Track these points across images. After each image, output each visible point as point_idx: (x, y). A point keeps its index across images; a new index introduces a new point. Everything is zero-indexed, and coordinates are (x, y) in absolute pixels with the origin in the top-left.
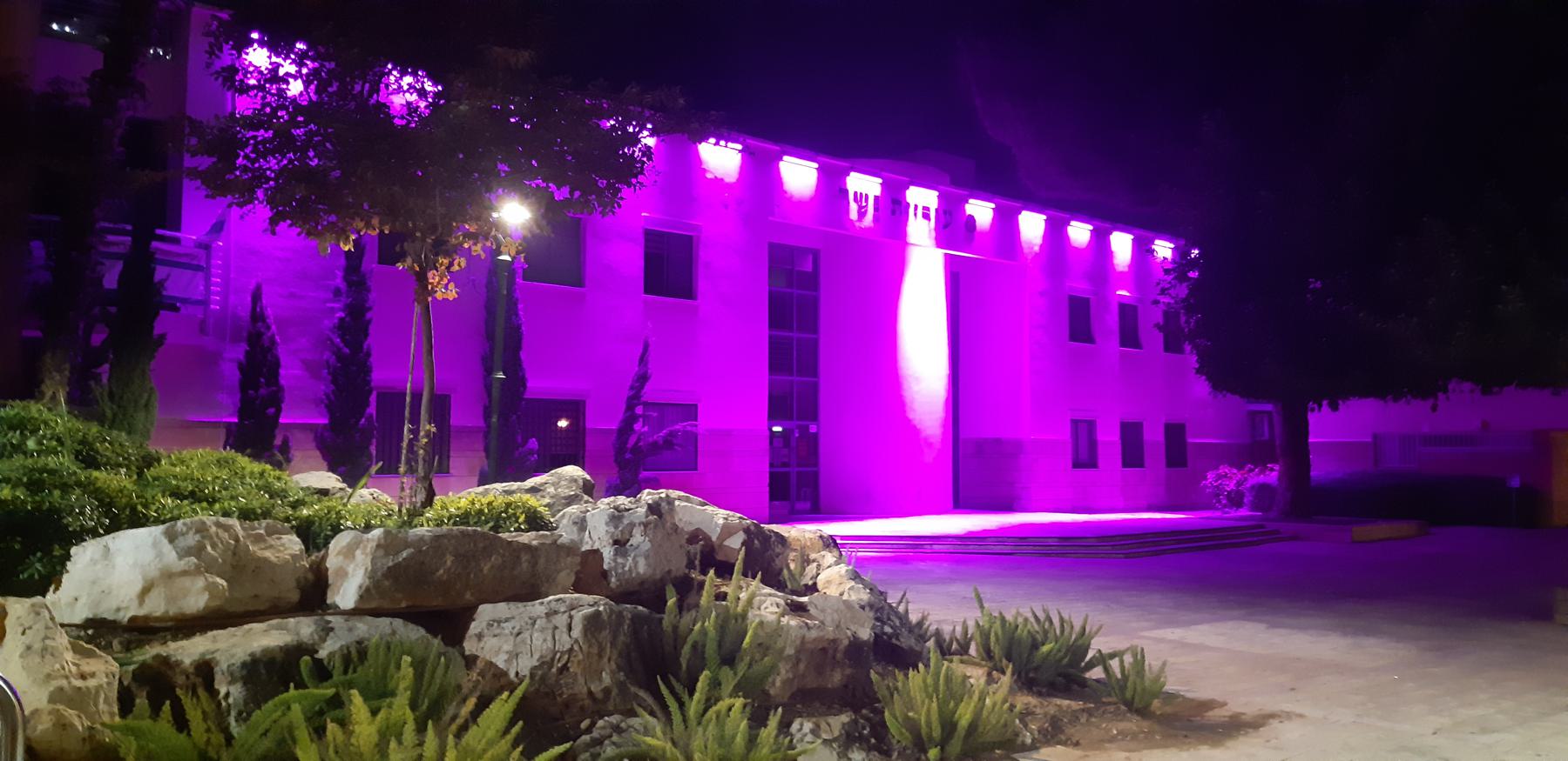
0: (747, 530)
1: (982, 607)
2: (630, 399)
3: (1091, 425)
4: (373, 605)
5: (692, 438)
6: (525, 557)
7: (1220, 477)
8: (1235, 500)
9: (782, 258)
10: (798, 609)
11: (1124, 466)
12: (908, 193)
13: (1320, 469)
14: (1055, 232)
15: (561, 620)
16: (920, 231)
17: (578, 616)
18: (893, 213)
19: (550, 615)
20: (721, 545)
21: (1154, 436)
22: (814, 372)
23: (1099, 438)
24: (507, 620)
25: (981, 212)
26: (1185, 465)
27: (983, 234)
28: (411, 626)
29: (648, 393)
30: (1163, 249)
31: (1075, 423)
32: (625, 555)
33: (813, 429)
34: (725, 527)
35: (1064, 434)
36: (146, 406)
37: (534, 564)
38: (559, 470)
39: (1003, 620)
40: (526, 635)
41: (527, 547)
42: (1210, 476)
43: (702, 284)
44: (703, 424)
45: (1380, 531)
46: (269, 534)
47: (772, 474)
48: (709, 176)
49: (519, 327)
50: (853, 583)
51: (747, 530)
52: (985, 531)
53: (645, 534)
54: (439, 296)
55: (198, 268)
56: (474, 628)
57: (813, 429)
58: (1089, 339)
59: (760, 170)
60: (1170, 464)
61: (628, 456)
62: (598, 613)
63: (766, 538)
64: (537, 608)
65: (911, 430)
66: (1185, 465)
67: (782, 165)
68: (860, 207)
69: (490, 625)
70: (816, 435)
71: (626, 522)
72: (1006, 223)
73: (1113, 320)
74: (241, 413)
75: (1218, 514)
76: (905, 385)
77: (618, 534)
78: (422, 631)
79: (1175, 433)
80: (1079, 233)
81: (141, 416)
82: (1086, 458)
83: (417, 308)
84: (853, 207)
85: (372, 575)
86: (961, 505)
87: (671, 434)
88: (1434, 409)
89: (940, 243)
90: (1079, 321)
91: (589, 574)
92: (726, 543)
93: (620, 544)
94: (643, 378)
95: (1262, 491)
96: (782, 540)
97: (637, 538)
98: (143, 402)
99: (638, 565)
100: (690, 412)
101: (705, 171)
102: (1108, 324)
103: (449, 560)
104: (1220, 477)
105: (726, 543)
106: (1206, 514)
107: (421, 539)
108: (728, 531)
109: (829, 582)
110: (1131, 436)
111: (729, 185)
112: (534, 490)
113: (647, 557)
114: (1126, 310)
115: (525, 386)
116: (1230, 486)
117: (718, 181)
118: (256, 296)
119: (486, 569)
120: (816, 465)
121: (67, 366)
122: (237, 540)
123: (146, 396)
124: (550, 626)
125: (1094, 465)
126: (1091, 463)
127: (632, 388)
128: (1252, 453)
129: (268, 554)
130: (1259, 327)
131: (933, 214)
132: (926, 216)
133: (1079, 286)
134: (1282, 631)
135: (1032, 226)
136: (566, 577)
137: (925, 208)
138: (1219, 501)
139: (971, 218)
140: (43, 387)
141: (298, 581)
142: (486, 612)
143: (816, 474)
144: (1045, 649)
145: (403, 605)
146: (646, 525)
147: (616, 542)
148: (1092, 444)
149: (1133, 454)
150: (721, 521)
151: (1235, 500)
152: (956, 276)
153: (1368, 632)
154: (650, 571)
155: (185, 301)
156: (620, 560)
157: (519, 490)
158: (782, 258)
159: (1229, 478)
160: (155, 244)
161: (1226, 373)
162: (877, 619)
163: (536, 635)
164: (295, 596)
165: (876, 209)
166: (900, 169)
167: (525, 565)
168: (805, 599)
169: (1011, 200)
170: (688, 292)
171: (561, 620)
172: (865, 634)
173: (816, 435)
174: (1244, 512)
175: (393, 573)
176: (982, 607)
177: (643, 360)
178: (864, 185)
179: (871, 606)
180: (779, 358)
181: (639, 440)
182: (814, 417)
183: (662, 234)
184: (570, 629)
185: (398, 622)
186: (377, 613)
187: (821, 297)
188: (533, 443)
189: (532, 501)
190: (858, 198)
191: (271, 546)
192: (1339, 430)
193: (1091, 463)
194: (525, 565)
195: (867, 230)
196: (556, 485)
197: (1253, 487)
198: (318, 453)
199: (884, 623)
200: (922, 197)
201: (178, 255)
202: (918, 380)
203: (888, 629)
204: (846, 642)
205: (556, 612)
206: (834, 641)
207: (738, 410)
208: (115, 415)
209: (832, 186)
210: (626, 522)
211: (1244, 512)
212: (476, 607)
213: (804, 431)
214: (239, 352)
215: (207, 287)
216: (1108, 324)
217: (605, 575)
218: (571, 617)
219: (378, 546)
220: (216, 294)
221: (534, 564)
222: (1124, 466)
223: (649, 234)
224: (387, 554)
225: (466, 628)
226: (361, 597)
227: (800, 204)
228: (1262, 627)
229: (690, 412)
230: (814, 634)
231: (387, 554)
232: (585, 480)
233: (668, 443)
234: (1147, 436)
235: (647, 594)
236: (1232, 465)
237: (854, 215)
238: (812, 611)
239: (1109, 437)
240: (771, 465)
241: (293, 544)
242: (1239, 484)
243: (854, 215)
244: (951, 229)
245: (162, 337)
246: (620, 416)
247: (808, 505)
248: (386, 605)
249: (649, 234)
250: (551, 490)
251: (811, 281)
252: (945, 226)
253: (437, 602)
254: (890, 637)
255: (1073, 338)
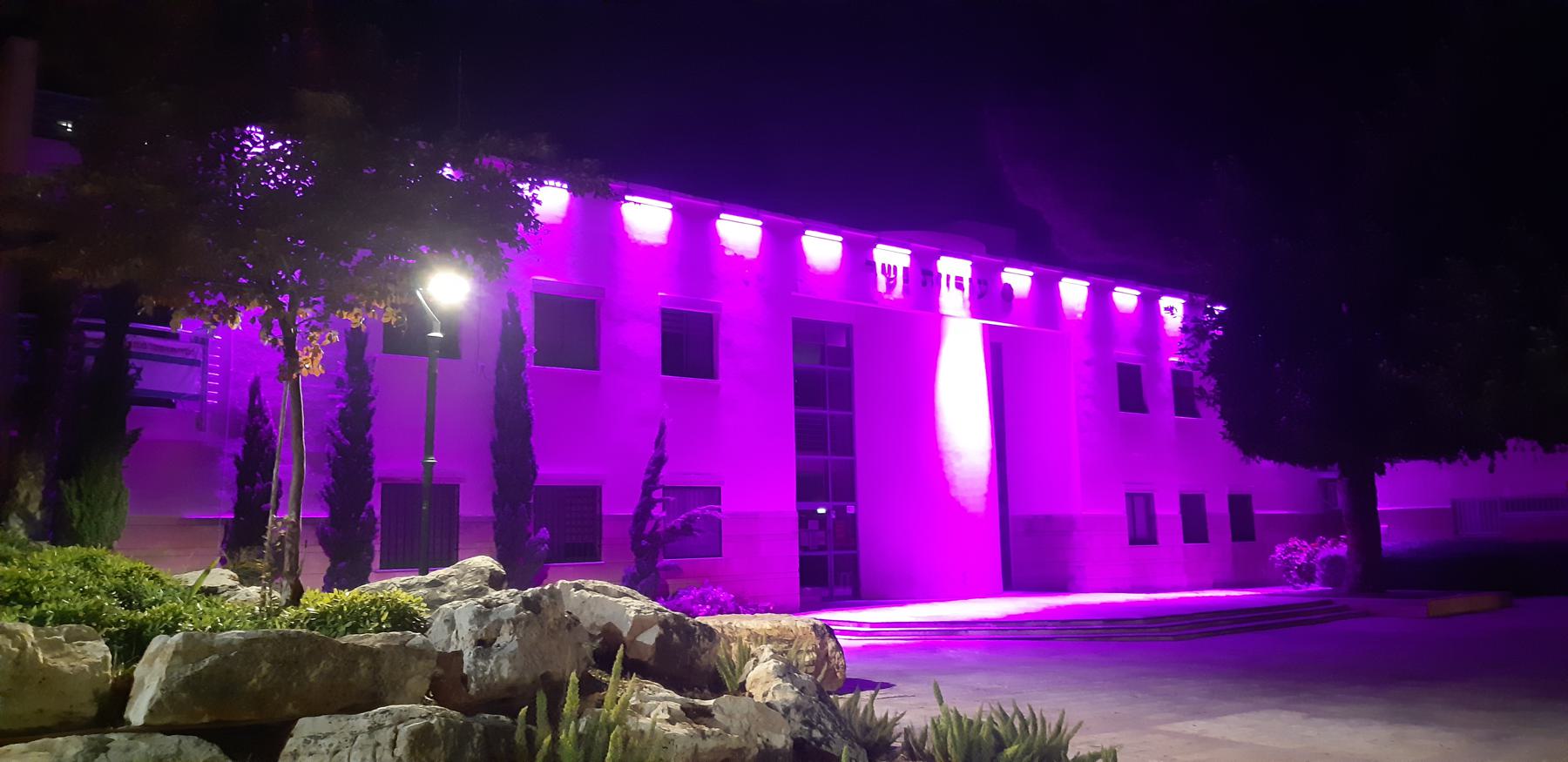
0: (664, 624)
1: (941, 703)
2: (646, 483)
3: (1148, 499)
4: (167, 720)
5: (714, 525)
6: (363, 663)
7: (1289, 550)
8: (1306, 574)
9: (806, 332)
10: (695, 715)
11: (1186, 541)
12: (875, 251)
13: (1391, 539)
14: (1099, 299)
15: (385, 736)
16: (953, 302)
17: (403, 730)
18: (924, 284)
19: (372, 730)
20: (633, 641)
21: (1217, 508)
22: (850, 451)
23: (605, 512)
24: (325, 736)
25: (1019, 280)
26: (1253, 539)
27: (1021, 300)
28: (205, 744)
29: (666, 476)
30: (1173, 311)
31: (1131, 497)
32: (486, 657)
33: (850, 509)
34: (636, 620)
35: (1120, 510)
36: (116, 504)
37: (375, 669)
38: (467, 561)
39: (959, 717)
40: (344, 753)
41: (368, 651)
42: (1279, 549)
43: (723, 363)
44: (728, 506)
45: (1457, 605)
46: (68, 640)
47: (801, 558)
48: (728, 253)
49: (529, 412)
50: (780, 681)
51: (664, 624)
52: (1026, 614)
53: (514, 632)
54: (304, 372)
55: (198, 363)
56: (291, 745)
57: (850, 509)
58: (1141, 407)
59: (782, 245)
60: (1236, 537)
61: (644, 543)
62: (429, 727)
63: (688, 633)
64: (361, 721)
65: (955, 506)
66: (1253, 539)
67: (805, 239)
68: (889, 279)
69: (306, 742)
70: (854, 516)
71: (492, 618)
72: (1045, 290)
73: (1166, 388)
74: (237, 510)
75: (1291, 590)
76: (946, 460)
77: (482, 633)
78: (216, 750)
79: (1240, 506)
80: (1126, 298)
81: (109, 514)
82: (1143, 533)
83: (287, 388)
84: (882, 279)
85: (165, 687)
86: (1011, 586)
87: (690, 519)
88: (1491, 470)
89: (975, 313)
90: (1130, 389)
91: (446, 679)
92: (639, 639)
93: (484, 645)
94: (659, 462)
95: (1333, 563)
96: (709, 633)
97: (505, 638)
98: (112, 500)
99: (500, 668)
100: (713, 495)
101: (723, 248)
102: (1161, 392)
103: (265, 667)
104: (1289, 550)
105: (639, 639)
106: (1278, 590)
107: (230, 644)
108: (640, 624)
109: (756, 680)
110: (1192, 507)
111: (750, 262)
112: (435, 584)
113: (512, 658)
114: (1179, 376)
115: (535, 474)
116: (1301, 559)
117: (738, 258)
118: (255, 390)
119: (313, 675)
120: (855, 547)
121: (42, 465)
122: (23, 647)
123: (115, 494)
124: (372, 742)
125: (1155, 542)
126: (1151, 540)
127: (648, 472)
128: (1317, 526)
129: (62, 664)
130: (1302, 387)
131: (966, 284)
132: (960, 286)
133: (1127, 353)
134: (1320, 721)
135: (1074, 293)
136: (418, 684)
137: (959, 279)
138: (1289, 576)
139: (1008, 287)
140: (18, 488)
141: (95, 693)
142: (306, 726)
143: (856, 558)
144: (1009, 751)
145: (206, 720)
146: (516, 622)
147: (480, 642)
148: (1151, 519)
149: (1195, 529)
150: (633, 614)
151: (1306, 574)
152: (997, 352)
153: (1418, 721)
154: (515, 676)
155: (178, 396)
156: (480, 663)
157: (419, 584)
158: (806, 332)
159: (1299, 551)
160: (129, 338)
161: (1254, 433)
162: (805, 723)
163: (354, 753)
164: (91, 711)
165: (906, 280)
166: (930, 233)
167: (363, 672)
168: (710, 702)
169: (1049, 263)
170: (709, 371)
171: (385, 736)
172: (780, 741)
173: (854, 516)
174: (1315, 587)
175: (192, 684)
176: (941, 703)
177: (659, 443)
178: (892, 257)
179: (798, 708)
180: (809, 436)
181: (657, 525)
182: (852, 498)
183: (681, 314)
184: (394, 744)
185: (189, 742)
186: (168, 730)
187: (853, 376)
188: (544, 532)
189: (404, 597)
190: (888, 270)
191: (69, 654)
192: (1408, 493)
193: (1151, 540)
194: (363, 672)
195: (897, 301)
196: (459, 578)
197: (1323, 560)
198: (320, 548)
199: (812, 727)
200: (954, 267)
201: (173, 350)
202: (958, 455)
203: (817, 734)
204: (755, 751)
205: (381, 726)
206: (740, 751)
207: (760, 487)
208: (83, 515)
209: (857, 261)
210: (492, 618)
211: (1315, 587)
212: (295, 722)
213: (840, 511)
214: (237, 447)
215: (204, 382)
216: (1161, 392)
217: (465, 680)
218: (396, 732)
219: (175, 653)
220: (213, 388)
221: (375, 669)
222: (1186, 541)
223: (664, 313)
224: (186, 662)
225: (282, 745)
226: (151, 711)
227: (1126, 315)
228: (1297, 716)
229: (713, 495)
230: (711, 743)
231: (186, 662)
232: (493, 572)
233: (687, 528)
234: (1210, 508)
235: (505, 699)
236: (1302, 538)
237: (882, 287)
238: (718, 716)
239: (1168, 512)
240: (801, 548)
241: (98, 650)
242: (1310, 557)
243: (882, 287)
244: (987, 297)
245: (136, 432)
246: (637, 501)
247: (849, 591)
248: (182, 720)
249: (664, 313)
250: (454, 583)
251: (845, 356)
252: (981, 296)
253: (248, 716)
254: (819, 743)
255: (1124, 407)
